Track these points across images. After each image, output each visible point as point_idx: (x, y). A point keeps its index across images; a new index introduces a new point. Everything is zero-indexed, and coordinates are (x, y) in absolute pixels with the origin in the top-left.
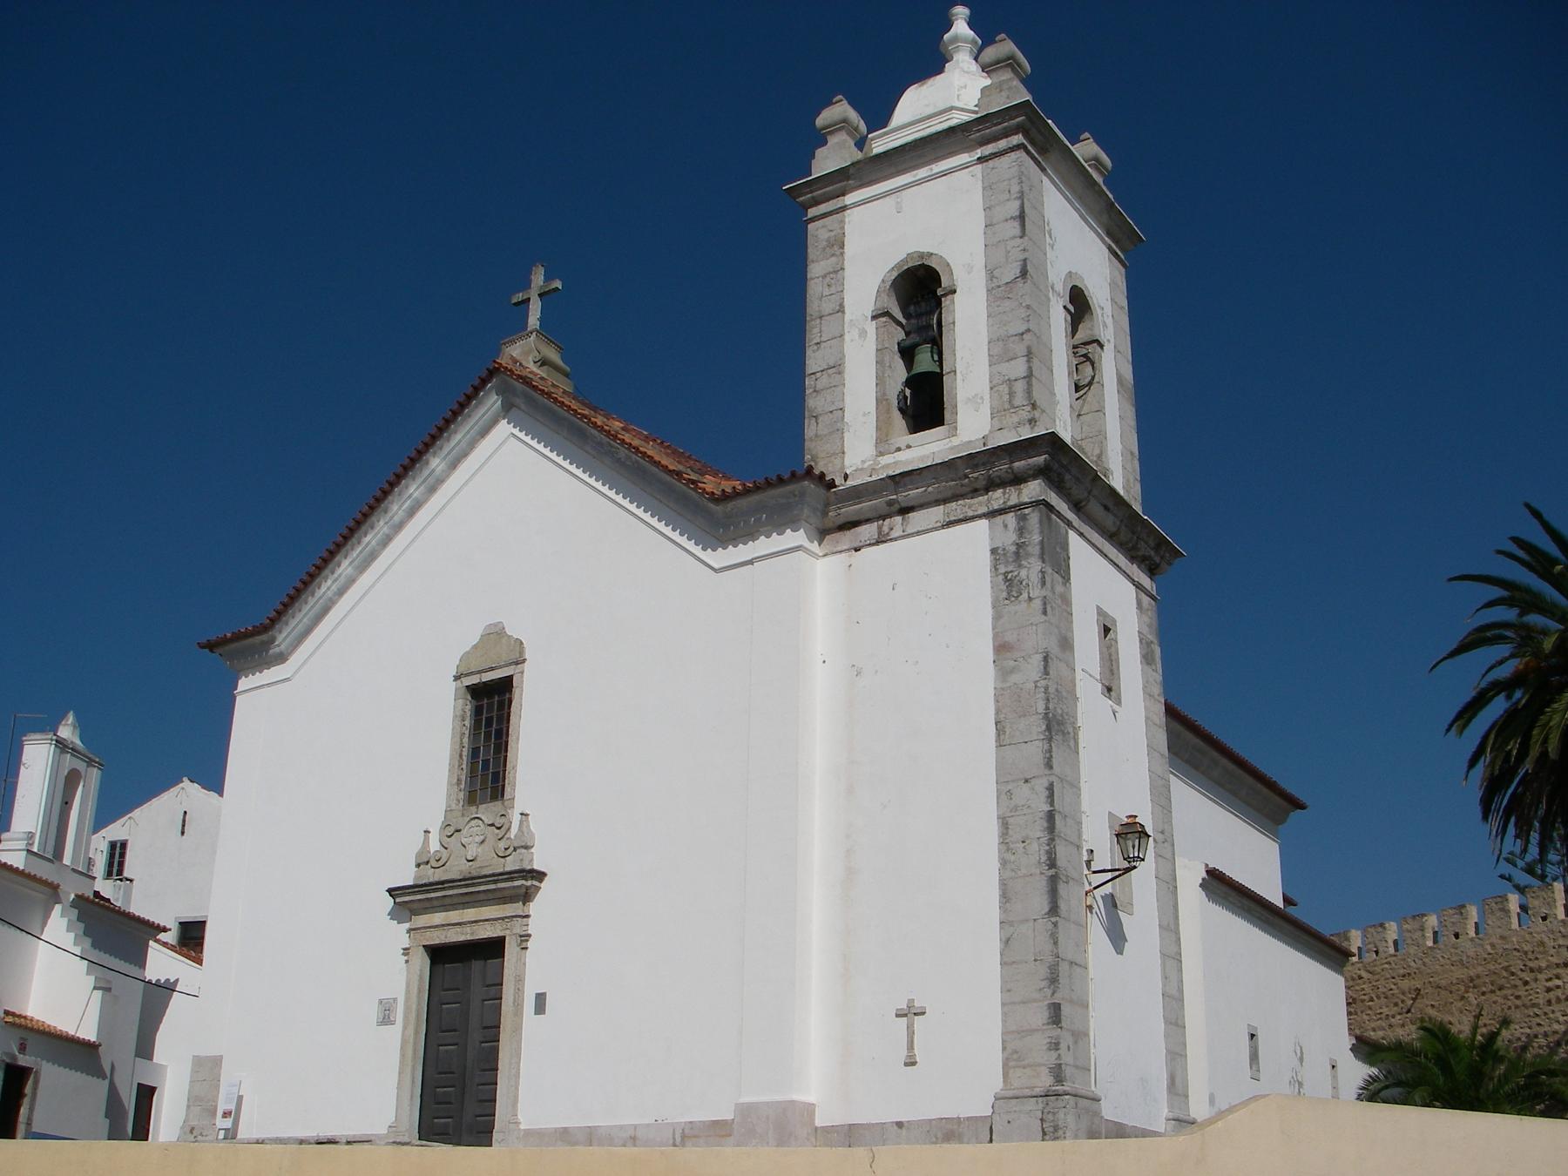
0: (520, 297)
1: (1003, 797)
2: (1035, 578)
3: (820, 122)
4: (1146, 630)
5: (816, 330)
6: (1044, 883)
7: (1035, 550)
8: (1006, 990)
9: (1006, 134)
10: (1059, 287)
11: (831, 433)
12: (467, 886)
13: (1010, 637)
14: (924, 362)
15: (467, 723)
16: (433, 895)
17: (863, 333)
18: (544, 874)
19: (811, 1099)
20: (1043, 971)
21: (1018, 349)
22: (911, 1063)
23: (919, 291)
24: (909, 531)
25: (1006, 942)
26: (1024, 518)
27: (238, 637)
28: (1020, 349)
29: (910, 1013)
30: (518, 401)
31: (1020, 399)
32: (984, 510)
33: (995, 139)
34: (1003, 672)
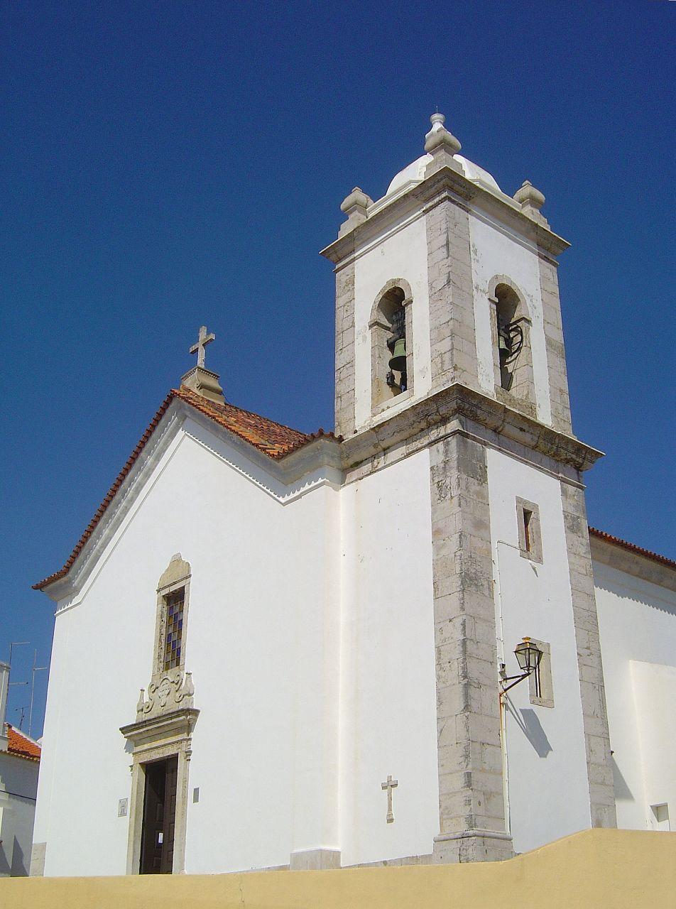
0: (194, 348)
1: (438, 633)
2: (454, 483)
3: (343, 207)
4: (571, 510)
5: (340, 341)
6: (461, 689)
7: (454, 464)
8: (441, 766)
9: (439, 193)
10: (485, 286)
11: (348, 406)
12: (158, 723)
13: (441, 525)
14: (399, 352)
15: (164, 619)
16: (141, 730)
17: (365, 338)
18: (198, 711)
19: (338, 848)
20: (461, 751)
21: (456, 332)
22: (390, 821)
23: (394, 303)
24: (387, 463)
25: (441, 732)
26: (447, 444)
27: (52, 580)
28: (447, 332)
29: (390, 785)
30: (188, 413)
31: (447, 366)
32: (426, 442)
33: (432, 197)
34: (437, 549)
